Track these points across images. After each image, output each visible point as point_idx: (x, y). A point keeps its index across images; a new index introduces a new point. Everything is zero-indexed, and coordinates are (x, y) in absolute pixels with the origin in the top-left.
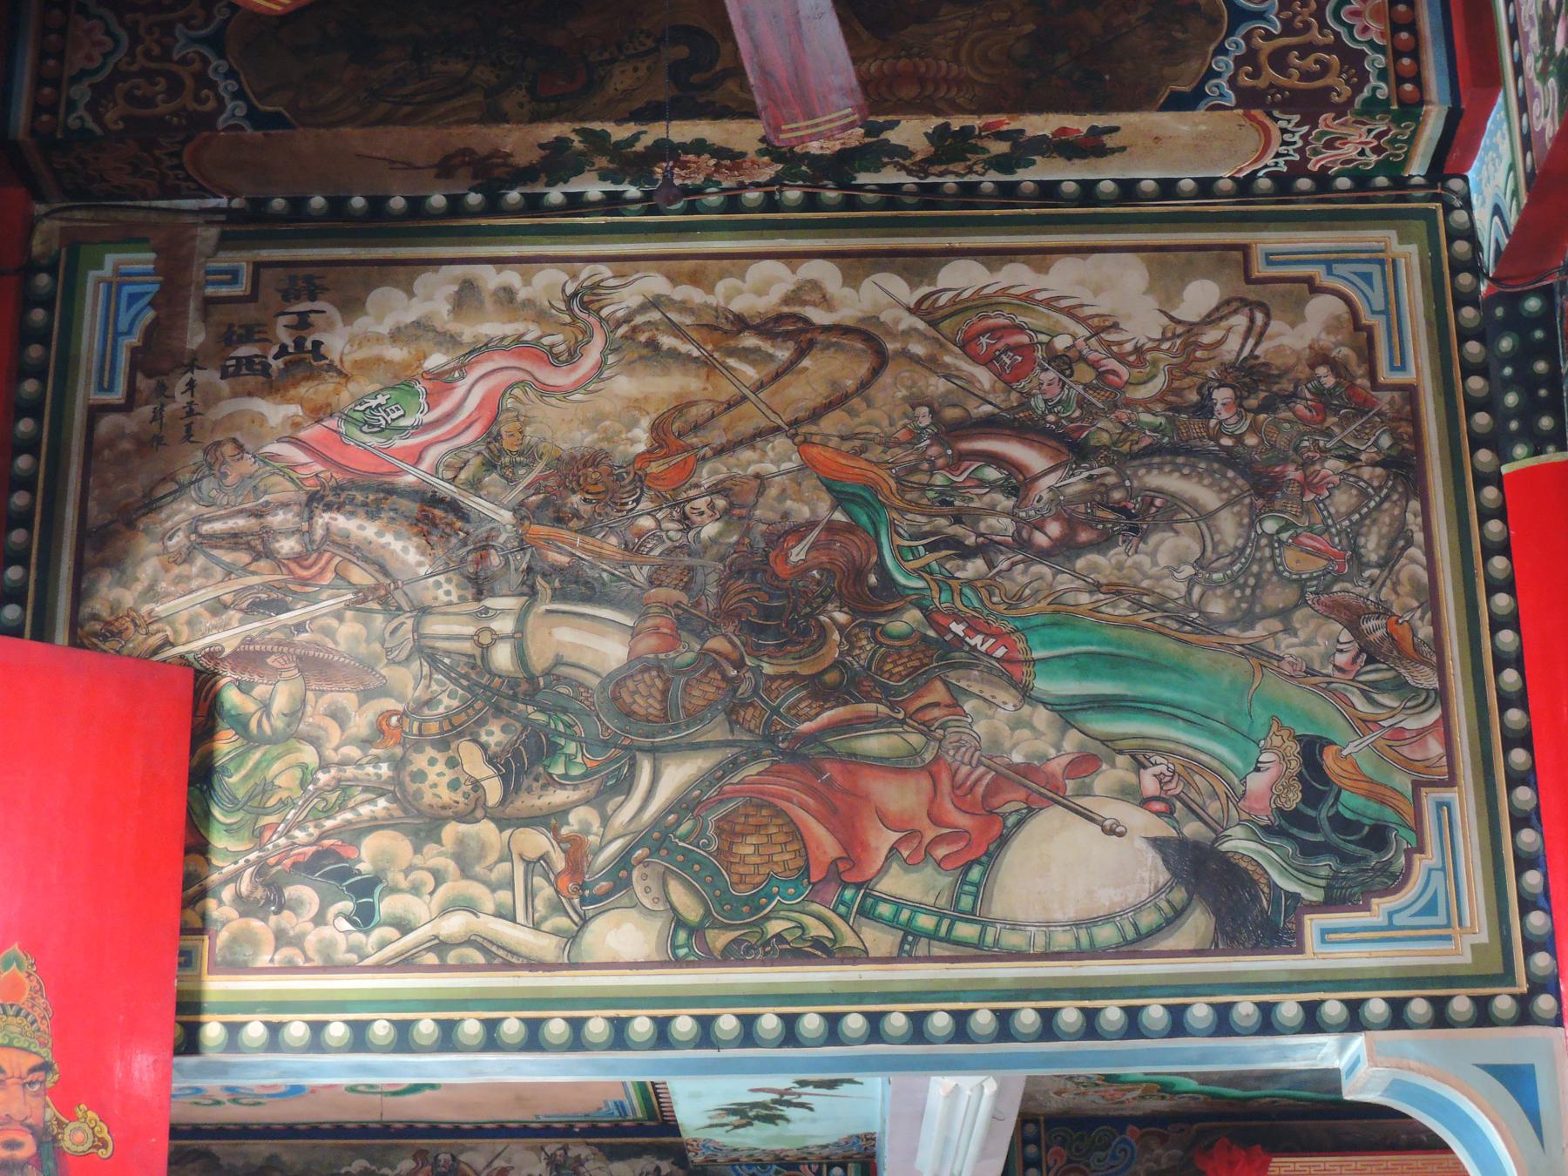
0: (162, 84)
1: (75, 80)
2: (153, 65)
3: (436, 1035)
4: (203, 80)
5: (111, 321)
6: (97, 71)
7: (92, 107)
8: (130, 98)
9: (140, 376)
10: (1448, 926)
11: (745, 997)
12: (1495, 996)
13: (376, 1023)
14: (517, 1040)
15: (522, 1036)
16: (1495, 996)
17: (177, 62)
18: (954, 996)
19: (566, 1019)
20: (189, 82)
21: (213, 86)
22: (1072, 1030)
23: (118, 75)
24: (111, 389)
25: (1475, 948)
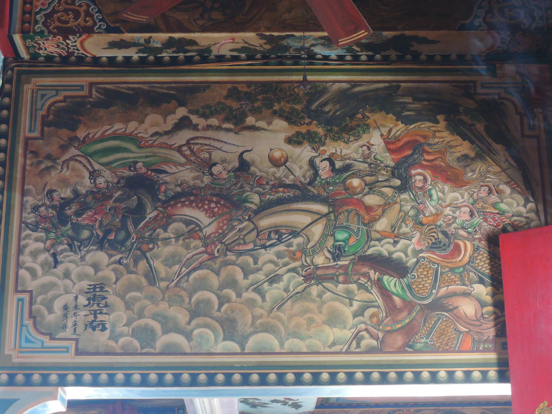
0: (71, 16)
1: (37, 13)
2: (67, 6)
3: (189, 380)
4: (88, 14)
5: (492, 85)
6: (46, 9)
7: (44, 24)
8: (59, 20)
9: (45, 128)
10: (20, 347)
11: (464, 364)
12: (422, 372)
13: (457, 372)
14: (56, 382)
15: (224, 378)
16: (422, 372)
17: (77, 6)
18: (242, 368)
19: (362, 372)
20: (83, 14)
21: (92, 16)
22: (291, 382)
23: (54, 11)
24: (34, 131)
25: (10, 356)
